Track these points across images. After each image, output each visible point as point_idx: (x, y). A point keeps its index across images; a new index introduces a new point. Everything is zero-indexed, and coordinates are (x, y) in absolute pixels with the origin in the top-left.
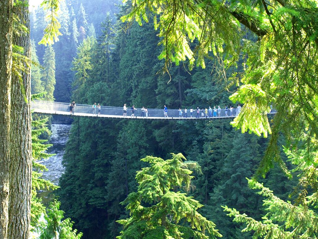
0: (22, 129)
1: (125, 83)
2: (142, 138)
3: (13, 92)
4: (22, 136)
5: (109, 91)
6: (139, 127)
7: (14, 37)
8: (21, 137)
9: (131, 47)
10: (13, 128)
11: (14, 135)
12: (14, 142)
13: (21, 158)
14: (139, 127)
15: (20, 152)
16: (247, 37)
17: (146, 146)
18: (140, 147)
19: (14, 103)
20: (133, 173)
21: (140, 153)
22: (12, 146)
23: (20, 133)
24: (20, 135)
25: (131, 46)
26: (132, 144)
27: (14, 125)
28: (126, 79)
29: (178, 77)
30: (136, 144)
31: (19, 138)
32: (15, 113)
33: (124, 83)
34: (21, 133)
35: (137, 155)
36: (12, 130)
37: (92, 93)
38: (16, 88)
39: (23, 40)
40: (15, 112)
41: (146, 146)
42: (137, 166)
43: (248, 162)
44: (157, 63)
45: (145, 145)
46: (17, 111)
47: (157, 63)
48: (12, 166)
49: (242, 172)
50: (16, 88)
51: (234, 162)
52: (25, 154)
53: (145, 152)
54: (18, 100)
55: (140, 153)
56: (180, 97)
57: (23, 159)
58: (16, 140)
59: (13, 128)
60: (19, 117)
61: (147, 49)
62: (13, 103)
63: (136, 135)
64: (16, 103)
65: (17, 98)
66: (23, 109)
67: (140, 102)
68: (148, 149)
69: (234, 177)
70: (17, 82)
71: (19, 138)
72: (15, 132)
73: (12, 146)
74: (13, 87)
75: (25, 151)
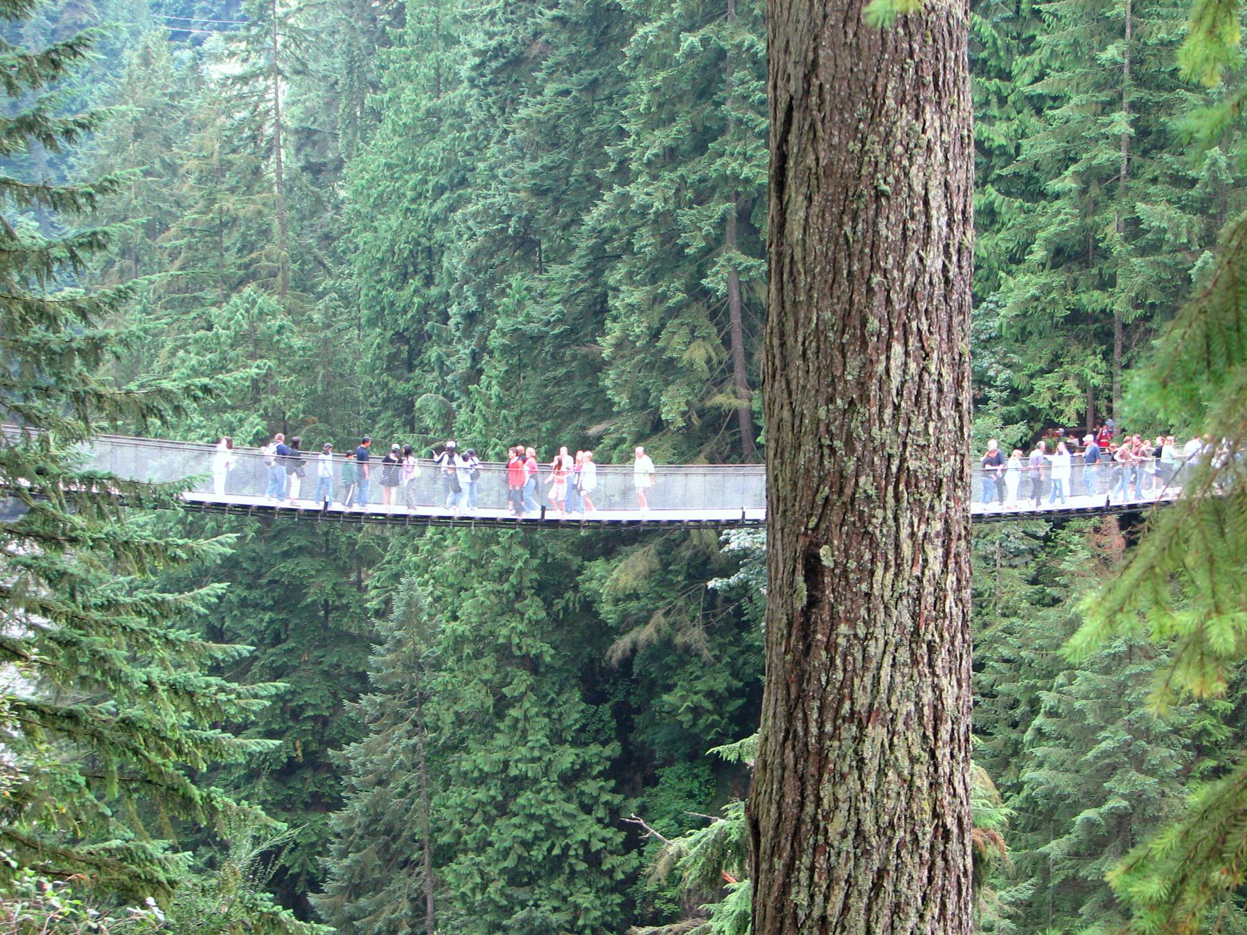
0: (941, 637)
1: (380, 292)
2: (517, 606)
3: (894, 392)
4: (944, 682)
5: (297, 342)
6: (498, 543)
7: (901, 31)
8: (935, 687)
9: (408, 93)
10: (890, 631)
11: (898, 679)
12: (900, 726)
13: (937, 826)
14: (498, 543)
15: (934, 785)
16: (1133, 27)
17: (539, 657)
18: (504, 653)
19: (899, 469)
20: (461, 805)
21: (505, 690)
22: (883, 753)
23: (931, 665)
24: (934, 674)
25: (411, 86)
26: (459, 641)
27: (895, 613)
28: (387, 274)
29: (730, 260)
30: (480, 641)
31: (928, 696)
32: (905, 532)
33: (373, 293)
34: (939, 663)
35: (490, 702)
36: (886, 643)
37: (198, 354)
38: (913, 366)
39: (951, 48)
40: (905, 522)
41: (539, 657)
42: (486, 769)
43: (1162, 738)
44: (611, 189)
45: (533, 652)
46: (916, 521)
47: (611, 189)
48: (888, 885)
49: (1138, 799)
50: (913, 366)
51: (1088, 736)
52: (958, 801)
53: (531, 688)
54: (923, 447)
55: (505, 690)
56: (739, 374)
57: (947, 835)
58: (908, 714)
59: (890, 631)
60: (925, 561)
61: (543, 104)
62: (894, 469)
63: (482, 590)
64: (912, 464)
65: (918, 434)
66: (948, 507)
67: (502, 405)
68: (550, 668)
69: (1090, 823)
70: (914, 324)
71: (925, 700)
72: (904, 655)
73: (883, 753)
74: (892, 362)
75: (956, 784)
